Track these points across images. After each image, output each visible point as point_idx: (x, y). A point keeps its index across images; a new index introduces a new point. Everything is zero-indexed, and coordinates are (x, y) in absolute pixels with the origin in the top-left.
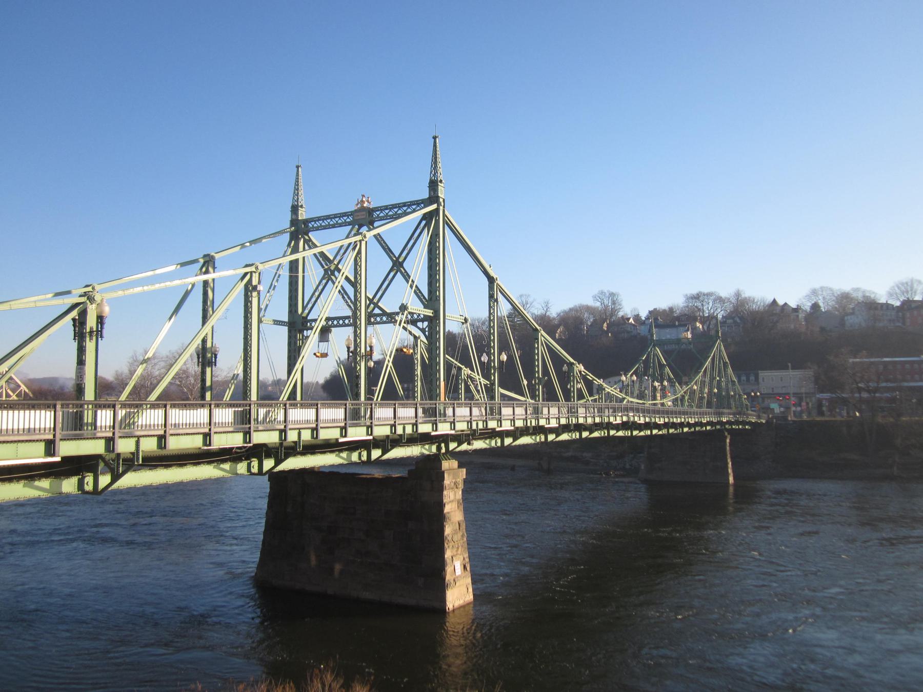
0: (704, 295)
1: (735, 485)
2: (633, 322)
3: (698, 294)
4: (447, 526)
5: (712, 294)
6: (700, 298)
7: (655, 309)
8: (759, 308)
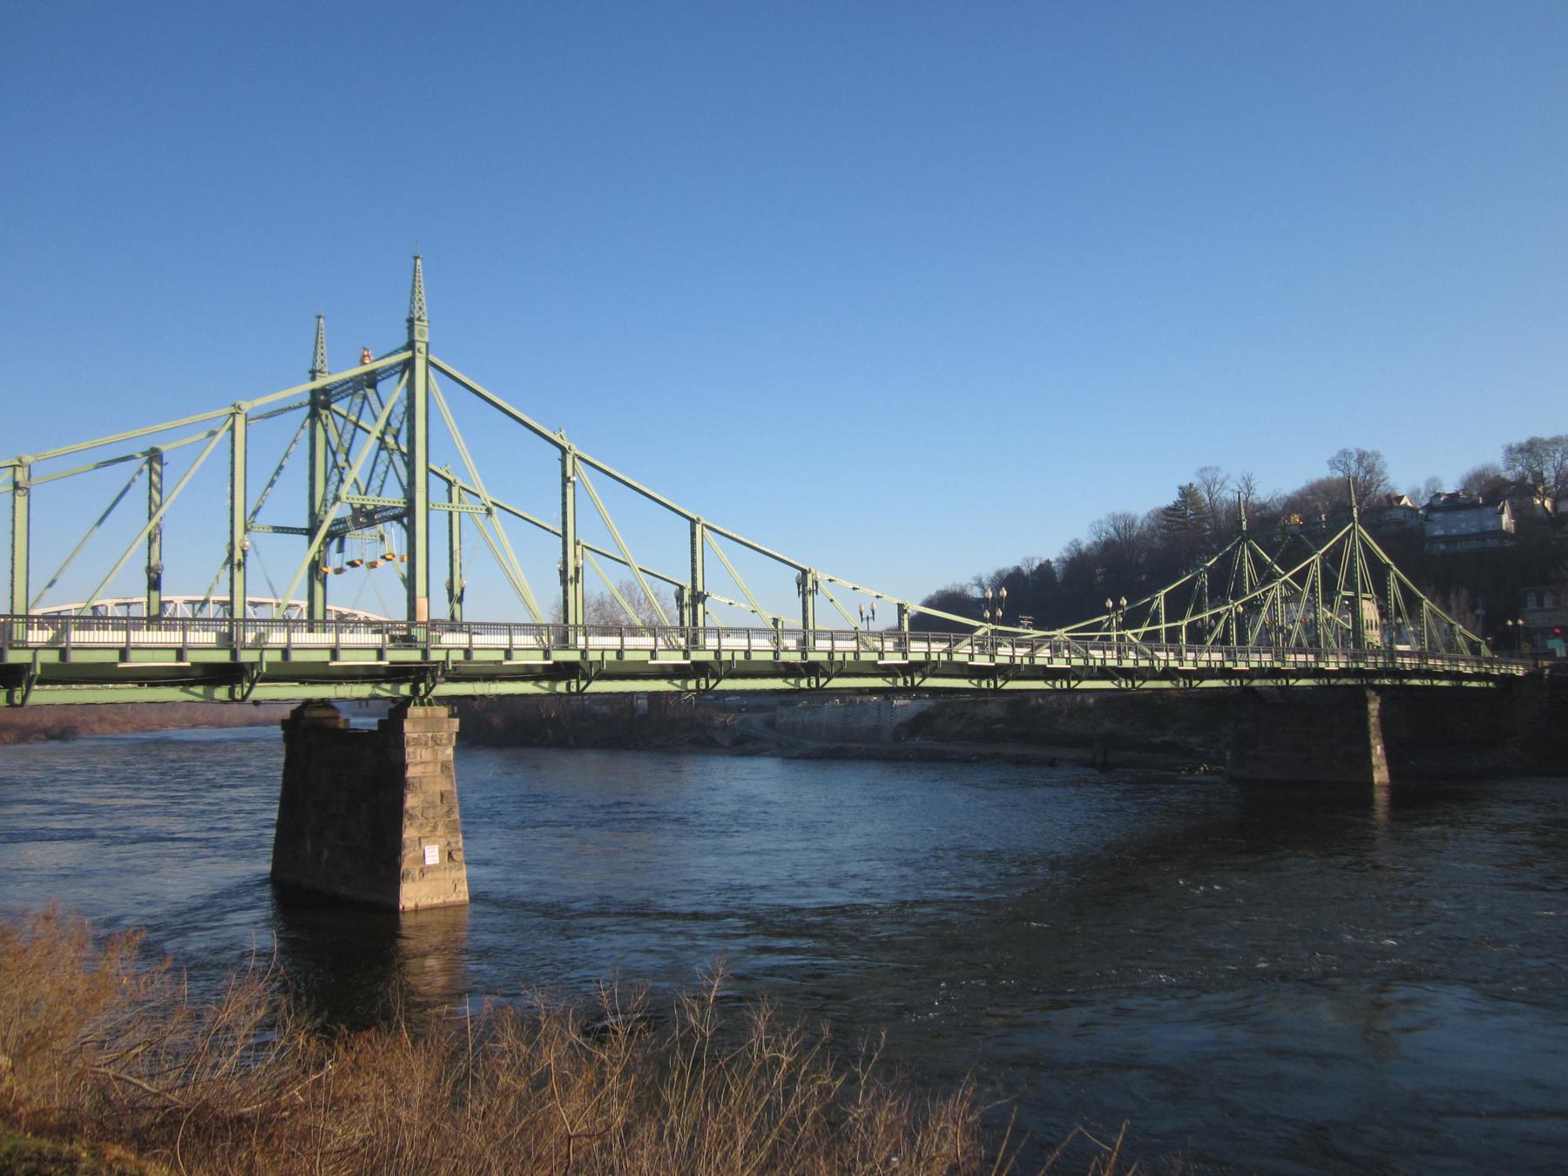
1: (1394, 788)
4: (409, 796)
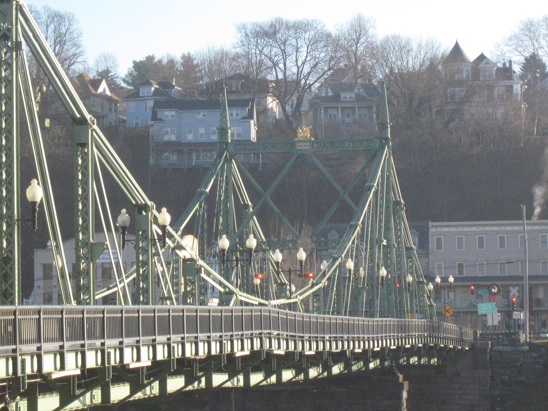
0: (288, 28)
2: (108, 93)
3: (272, 25)
5: (307, 25)
6: (279, 36)
7: (150, 59)
8: (421, 66)
